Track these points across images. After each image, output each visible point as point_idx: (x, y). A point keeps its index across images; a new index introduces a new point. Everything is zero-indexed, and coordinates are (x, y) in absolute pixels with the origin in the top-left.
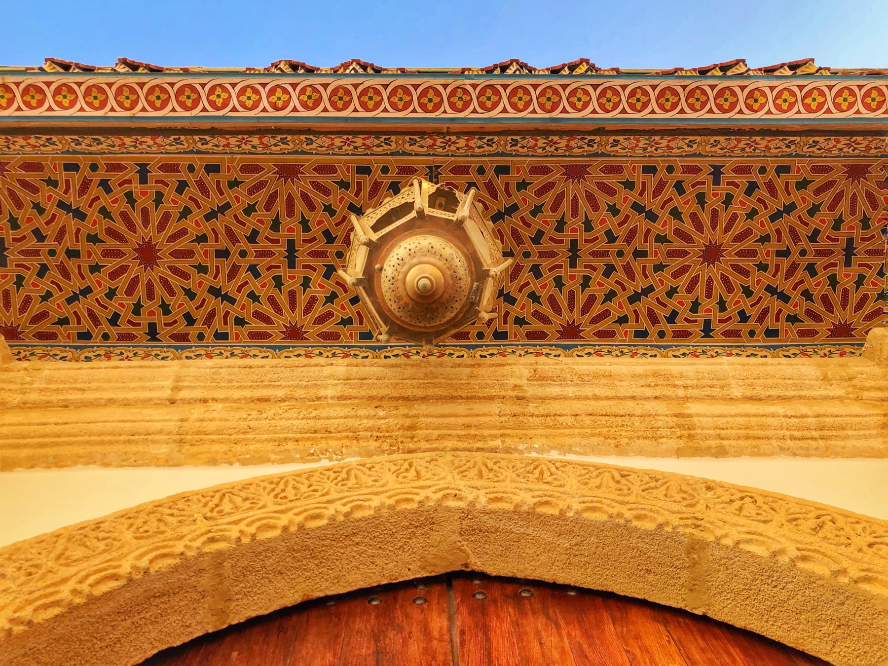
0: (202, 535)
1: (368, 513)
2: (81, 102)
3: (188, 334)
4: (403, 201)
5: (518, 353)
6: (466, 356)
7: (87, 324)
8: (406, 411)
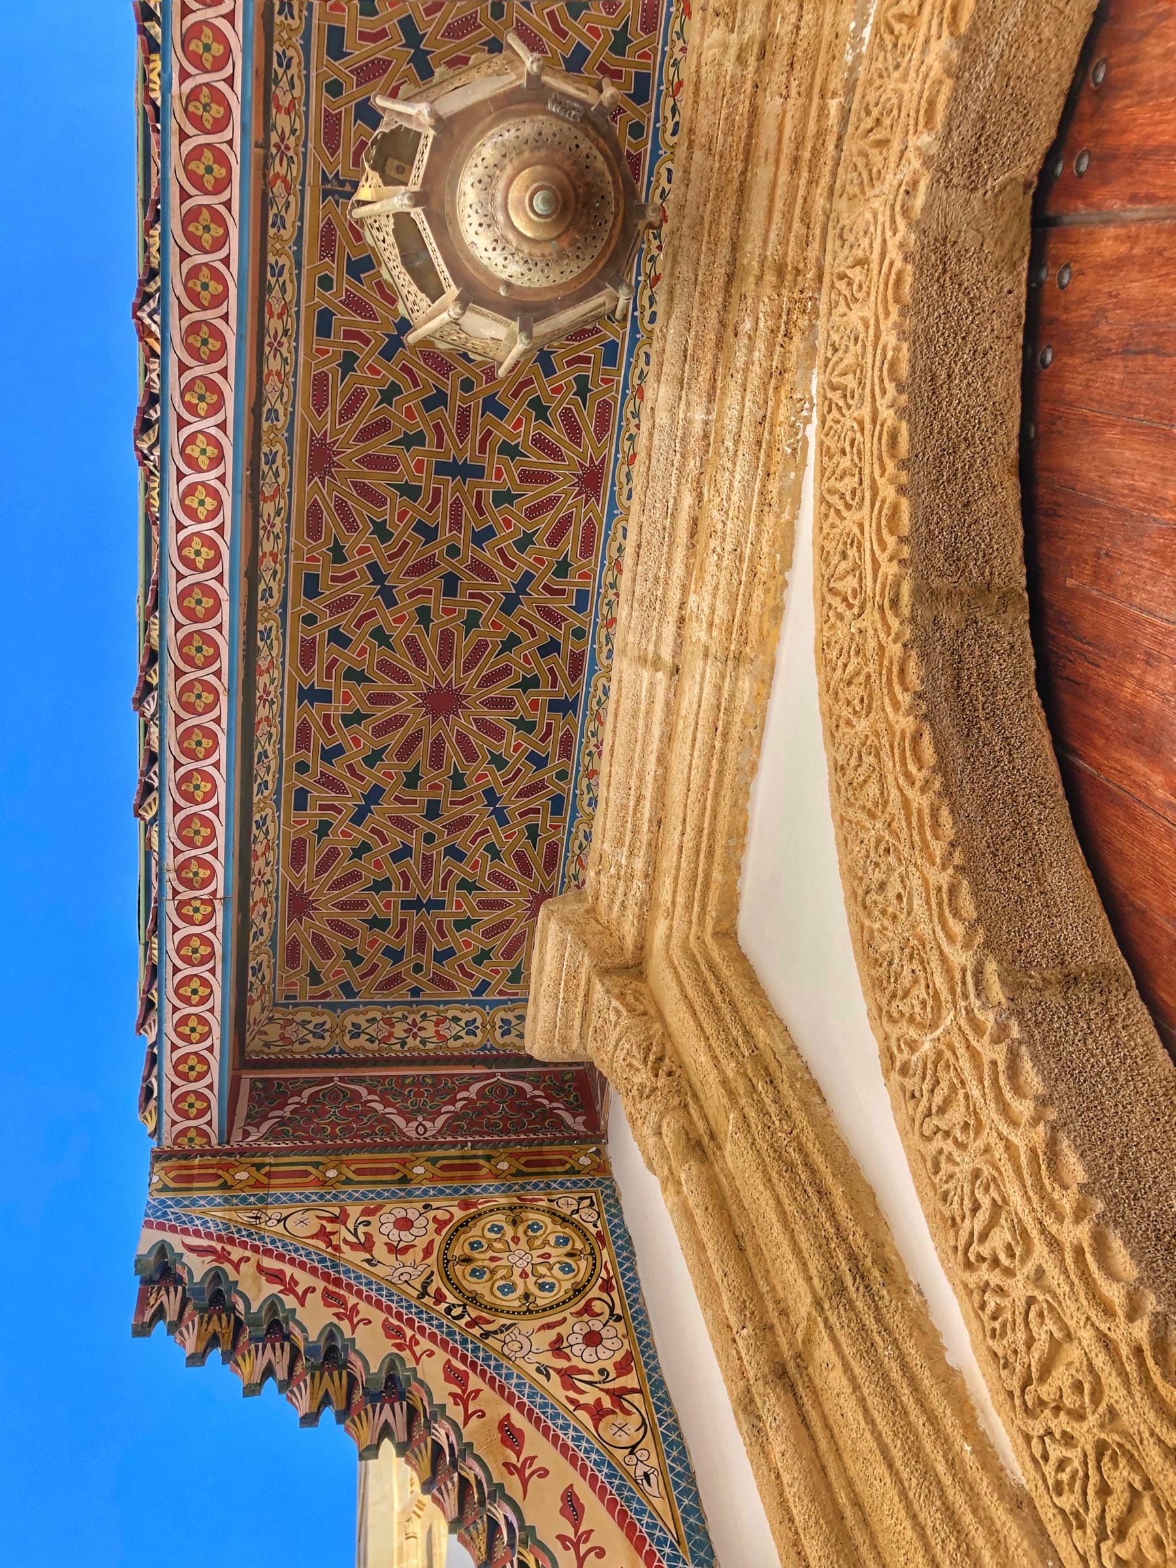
0: (884, 618)
1: (905, 354)
2: (206, 765)
3: (573, 653)
4: (391, 239)
5: (678, 55)
6: (669, 165)
7: (540, 800)
8: (752, 280)
